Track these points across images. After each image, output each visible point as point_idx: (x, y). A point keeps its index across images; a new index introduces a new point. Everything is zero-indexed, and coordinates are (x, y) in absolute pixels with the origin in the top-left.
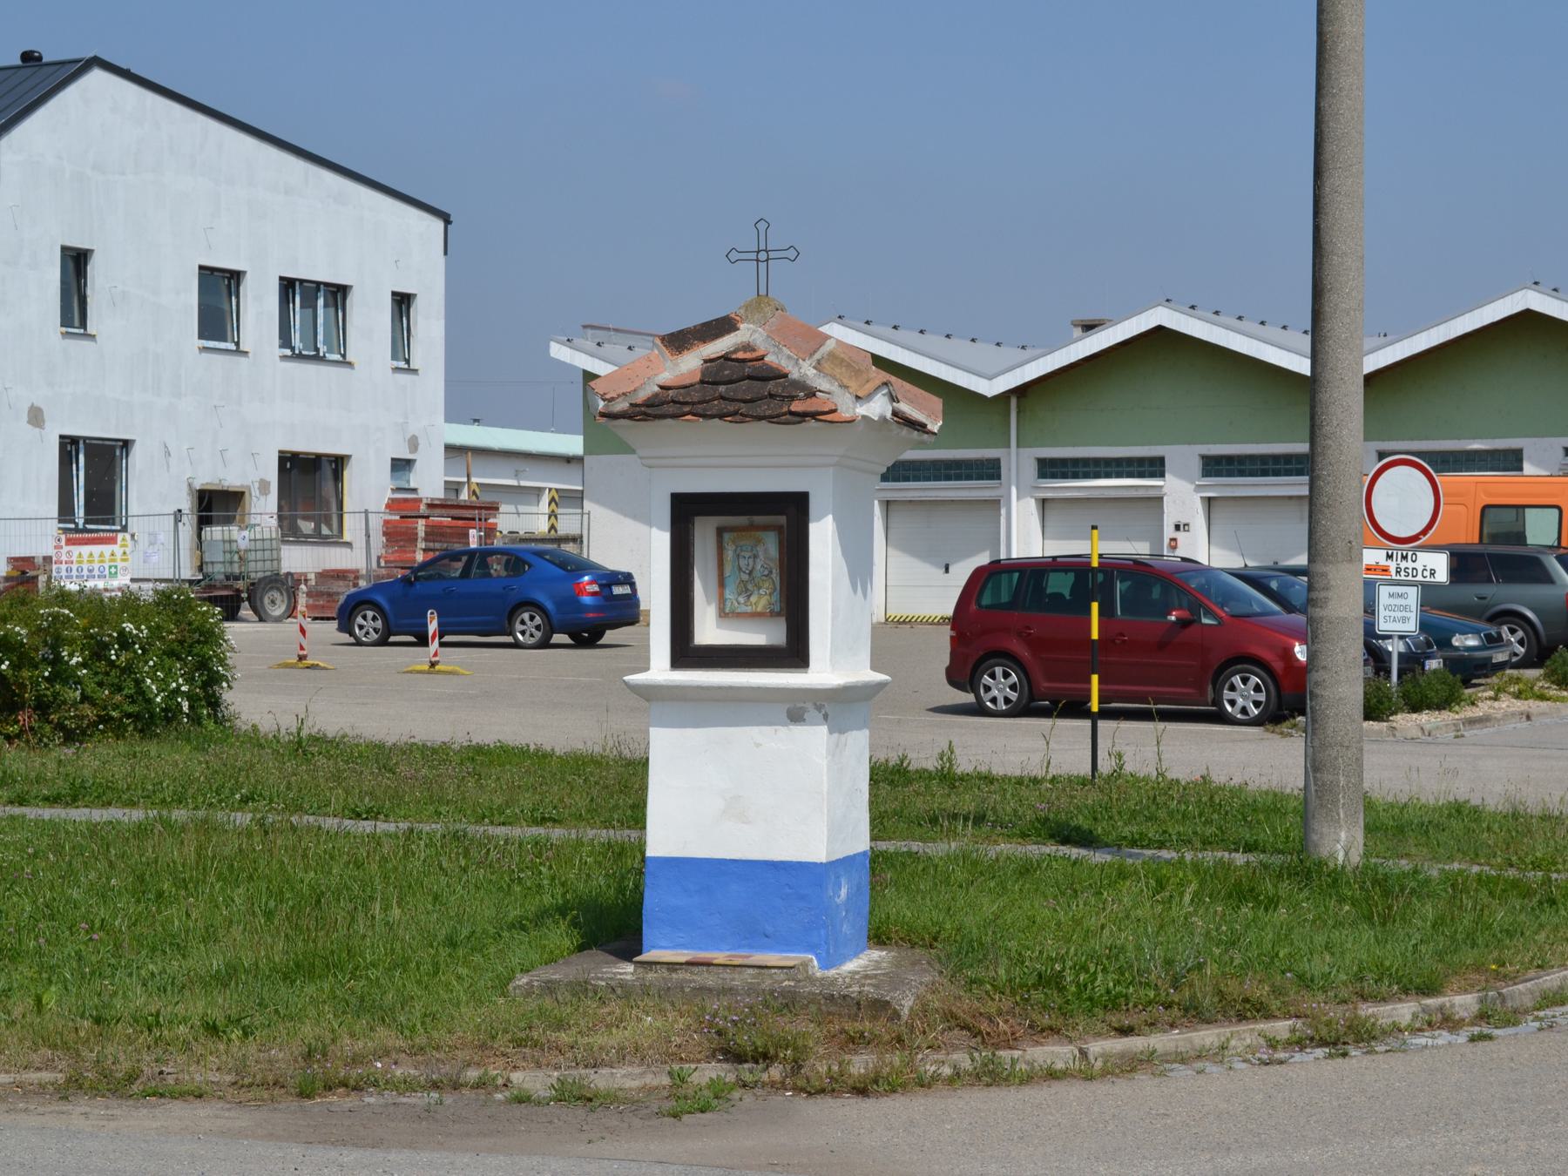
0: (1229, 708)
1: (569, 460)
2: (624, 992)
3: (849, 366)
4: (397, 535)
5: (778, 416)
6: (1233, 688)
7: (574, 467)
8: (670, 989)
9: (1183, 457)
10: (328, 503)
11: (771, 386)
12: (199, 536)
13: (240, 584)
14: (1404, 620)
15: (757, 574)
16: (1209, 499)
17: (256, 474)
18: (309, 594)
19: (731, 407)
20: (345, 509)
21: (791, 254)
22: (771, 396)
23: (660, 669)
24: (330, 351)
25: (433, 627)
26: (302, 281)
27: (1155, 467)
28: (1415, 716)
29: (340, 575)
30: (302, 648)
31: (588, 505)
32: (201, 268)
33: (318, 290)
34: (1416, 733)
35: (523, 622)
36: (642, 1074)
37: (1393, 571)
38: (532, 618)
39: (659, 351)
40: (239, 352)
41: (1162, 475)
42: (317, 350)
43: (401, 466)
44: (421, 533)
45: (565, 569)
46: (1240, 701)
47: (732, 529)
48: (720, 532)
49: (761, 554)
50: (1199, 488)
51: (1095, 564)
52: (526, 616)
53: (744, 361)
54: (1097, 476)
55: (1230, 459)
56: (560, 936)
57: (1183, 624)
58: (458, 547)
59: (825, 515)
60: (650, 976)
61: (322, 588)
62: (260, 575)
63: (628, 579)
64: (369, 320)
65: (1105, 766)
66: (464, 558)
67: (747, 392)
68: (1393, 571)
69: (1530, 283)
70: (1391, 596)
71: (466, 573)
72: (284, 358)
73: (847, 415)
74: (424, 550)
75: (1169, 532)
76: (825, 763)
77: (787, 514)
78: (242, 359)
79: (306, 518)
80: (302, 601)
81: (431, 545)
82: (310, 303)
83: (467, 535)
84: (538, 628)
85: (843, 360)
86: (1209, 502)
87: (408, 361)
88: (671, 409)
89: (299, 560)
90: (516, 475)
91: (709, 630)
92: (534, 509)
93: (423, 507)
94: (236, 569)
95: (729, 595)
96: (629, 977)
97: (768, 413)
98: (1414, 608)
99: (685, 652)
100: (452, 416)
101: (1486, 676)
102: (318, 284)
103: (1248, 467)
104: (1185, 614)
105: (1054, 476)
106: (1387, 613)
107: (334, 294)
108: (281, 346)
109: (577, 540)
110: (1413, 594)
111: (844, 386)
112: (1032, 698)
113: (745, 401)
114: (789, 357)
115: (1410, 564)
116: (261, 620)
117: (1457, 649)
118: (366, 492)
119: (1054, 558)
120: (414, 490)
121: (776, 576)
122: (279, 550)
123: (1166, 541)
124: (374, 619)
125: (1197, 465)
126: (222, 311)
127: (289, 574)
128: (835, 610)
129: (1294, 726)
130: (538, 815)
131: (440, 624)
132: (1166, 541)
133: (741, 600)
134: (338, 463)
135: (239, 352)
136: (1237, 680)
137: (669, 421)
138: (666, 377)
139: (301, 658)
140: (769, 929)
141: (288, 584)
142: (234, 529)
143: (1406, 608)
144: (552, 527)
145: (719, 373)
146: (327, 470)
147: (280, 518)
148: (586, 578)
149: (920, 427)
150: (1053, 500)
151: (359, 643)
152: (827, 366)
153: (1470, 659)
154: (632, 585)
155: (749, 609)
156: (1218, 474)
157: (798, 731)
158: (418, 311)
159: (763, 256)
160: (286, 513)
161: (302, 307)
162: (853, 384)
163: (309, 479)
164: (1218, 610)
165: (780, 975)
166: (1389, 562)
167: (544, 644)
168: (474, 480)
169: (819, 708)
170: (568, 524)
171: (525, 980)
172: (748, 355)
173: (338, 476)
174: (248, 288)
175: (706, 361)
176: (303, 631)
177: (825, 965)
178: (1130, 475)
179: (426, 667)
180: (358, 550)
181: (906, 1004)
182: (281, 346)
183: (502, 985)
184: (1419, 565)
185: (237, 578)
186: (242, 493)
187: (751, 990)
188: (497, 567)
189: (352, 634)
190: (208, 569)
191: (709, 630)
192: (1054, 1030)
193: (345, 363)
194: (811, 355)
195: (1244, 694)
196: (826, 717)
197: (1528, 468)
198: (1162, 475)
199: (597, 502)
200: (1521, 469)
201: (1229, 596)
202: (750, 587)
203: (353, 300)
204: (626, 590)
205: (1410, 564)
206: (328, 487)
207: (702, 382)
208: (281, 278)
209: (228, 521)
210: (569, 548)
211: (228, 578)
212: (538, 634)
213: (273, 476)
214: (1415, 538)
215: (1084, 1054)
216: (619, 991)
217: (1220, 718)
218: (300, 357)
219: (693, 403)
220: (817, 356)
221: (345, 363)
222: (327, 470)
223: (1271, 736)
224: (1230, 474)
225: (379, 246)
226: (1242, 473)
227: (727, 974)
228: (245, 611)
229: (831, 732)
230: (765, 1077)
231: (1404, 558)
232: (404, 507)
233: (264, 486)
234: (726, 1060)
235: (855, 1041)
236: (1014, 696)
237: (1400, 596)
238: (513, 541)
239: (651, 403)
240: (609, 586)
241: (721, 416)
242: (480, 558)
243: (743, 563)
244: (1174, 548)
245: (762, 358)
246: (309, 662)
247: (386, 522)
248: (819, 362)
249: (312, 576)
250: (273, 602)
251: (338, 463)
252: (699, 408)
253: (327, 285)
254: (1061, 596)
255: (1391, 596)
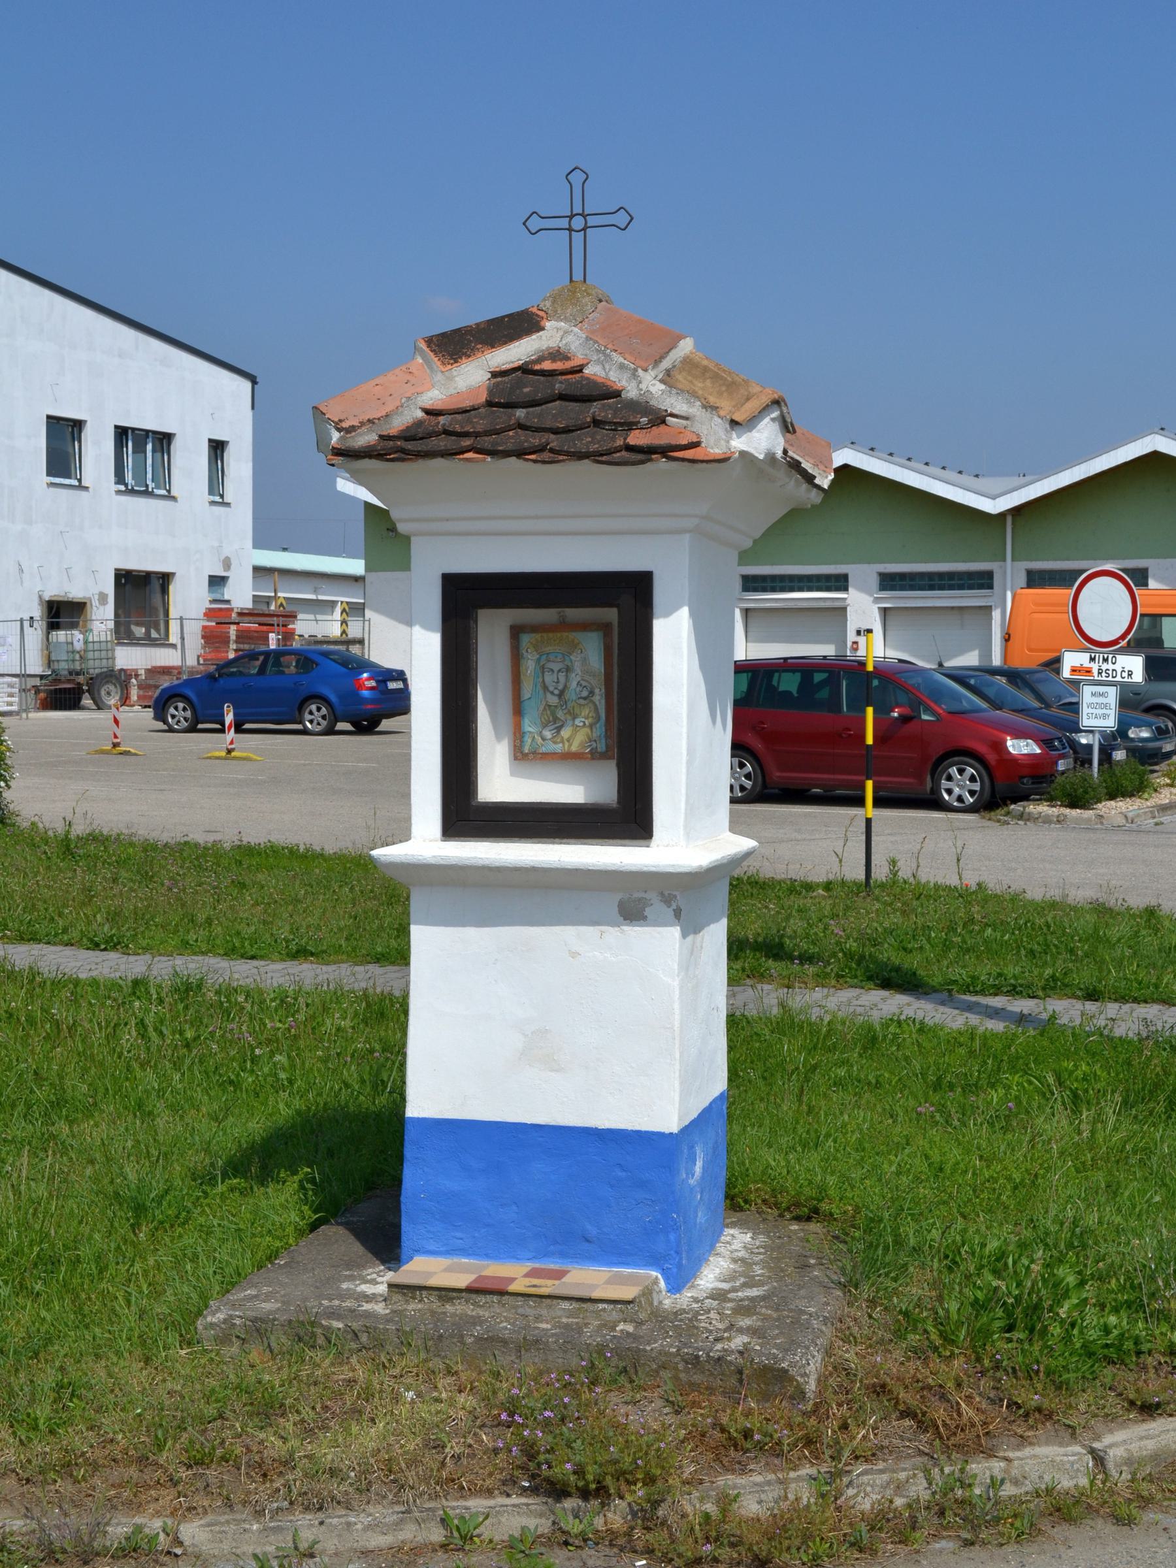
0: (946, 797)
1: (357, 579)
2: (369, 1340)
3: (716, 377)
4: (213, 638)
5: (609, 452)
6: (950, 778)
7: (360, 584)
8: (438, 1336)
9: (864, 573)
10: (156, 609)
11: (595, 408)
12: (48, 639)
13: (81, 679)
14: (1105, 716)
15: (571, 695)
16: (885, 609)
17: (95, 586)
18: (140, 687)
19: (535, 440)
20: (171, 616)
21: (621, 219)
22: (597, 423)
23: (425, 841)
24: (158, 487)
25: (229, 718)
26: (133, 429)
27: (840, 582)
28: (1112, 802)
29: (166, 671)
30: (116, 737)
31: (368, 613)
32: (49, 417)
33: (147, 437)
34: (1121, 821)
35: (311, 713)
36: (398, 1525)
37: (1095, 672)
38: (319, 709)
39: (422, 361)
40: (81, 487)
41: (846, 589)
42: (147, 486)
43: (217, 582)
44: (233, 637)
45: (347, 667)
46: (957, 790)
47: (534, 629)
48: (516, 632)
49: (577, 667)
50: (877, 600)
51: (870, 668)
52: (314, 707)
53: (552, 373)
54: (792, 590)
55: (902, 576)
56: (283, 1201)
57: (905, 720)
58: (263, 648)
59: (677, 608)
60: (413, 1306)
61: (151, 682)
62: (97, 671)
63: (400, 676)
64: (189, 464)
65: (880, 872)
66: (261, 658)
67: (558, 419)
68: (1095, 672)
69: (1157, 429)
70: (1093, 695)
71: (262, 670)
72: (119, 492)
73: (716, 451)
74: (236, 651)
75: (851, 636)
76: (676, 983)
77: (626, 600)
78: (84, 493)
79: (138, 624)
80: (134, 694)
81: (241, 646)
82: (140, 449)
83: (268, 638)
84: (324, 717)
85: (706, 369)
86: (885, 612)
87: (222, 496)
88: (442, 443)
89: (130, 658)
90: (315, 591)
91: (499, 781)
92: (329, 618)
93: (234, 615)
94: (77, 666)
95: (528, 726)
96: (380, 1308)
97: (594, 447)
98: (1113, 706)
99: (464, 814)
100: (259, 543)
101: (1156, 764)
102: (147, 432)
103: (937, 582)
104: (907, 711)
105: (755, 590)
106: (1090, 711)
107: (161, 441)
108: (116, 483)
109: (361, 642)
110: (1112, 692)
111: (709, 407)
112: (765, 785)
113: (556, 431)
114: (622, 367)
115: (1110, 666)
116: (99, 708)
117: (1132, 740)
118: (188, 603)
119: (785, 659)
120: (228, 602)
121: (599, 698)
122: (113, 650)
123: (849, 644)
124: (184, 709)
125: (874, 581)
126: (67, 453)
127: (122, 670)
128: (690, 751)
129: (1008, 813)
130: (293, 947)
131: (235, 715)
132: (849, 644)
133: (548, 734)
134: (165, 579)
135: (81, 487)
136: (954, 771)
137: (439, 462)
138: (434, 397)
139: (115, 745)
140: (592, 1230)
141: (121, 679)
142: (76, 632)
143: (1106, 706)
144: (344, 632)
145: (509, 390)
146: (156, 584)
147: (117, 624)
148: (365, 675)
149: (809, 478)
150: (754, 609)
151: (171, 730)
152: (680, 378)
153: (1143, 749)
154: (405, 681)
155: (558, 748)
156: (893, 588)
157: (635, 934)
158: (230, 455)
159: (578, 223)
160: (122, 619)
161: (134, 452)
162: (726, 405)
163: (141, 592)
164: (936, 707)
165: (613, 1313)
166: (1092, 665)
167: (330, 731)
168: (279, 594)
169: (667, 900)
170: (354, 631)
171: (221, 1316)
172: (559, 366)
173: (165, 590)
174: (88, 434)
175: (495, 375)
176: (116, 721)
177: (676, 1287)
178: (819, 589)
179: (223, 754)
180: (183, 649)
181: (810, 1369)
182: (116, 483)
183: (184, 1324)
184: (1118, 667)
185: (78, 674)
186: (85, 604)
187: (570, 1337)
188: (291, 666)
189: (165, 722)
190: (56, 666)
191: (499, 781)
192: (1045, 1415)
193: (170, 497)
194: (657, 363)
195: (960, 783)
196: (678, 914)
197: (1152, 584)
198: (846, 589)
199: (377, 610)
200: (1147, 585)
201: (938, 693)
202: (560, 714)
203: (177, 446)
204: (400, 685)
205: (1110, 666)
206: (157, 599)
207: (490, 404)
208: (116, 427)
209: (73, 626)
210: (355, 650)
211: (71, 673)
212: (324, 723)
213: (110, 590)
214: (1114, 642)
215: (1099, 1459)
216: (364, 1338)
217: (934, 803)
218: (131, 492)
219: (477, 435)
220: (666, 364)
221: (170, 497)
222: (156, 584)
223: (989, 823)
224: (902, 588)
225: (201, 402)
226: (912, 588)
227: (529, 1309)
228: (87, 701)
229: (684, 935)
230: (599, 1522)
231: (1105, 660)
232: (219, 615)
233: (103, 598)
234: (534, 1491)
235: (735, 1447)
236: (748, 784)
237: (1101, 695)
238: (309, 643)
239: (411, 435)
240: (384, 682)
241: (520, 454)
242: (276, 657)
243: (549, 679)
244: (856, 649)
245: (579, 370)
246: (122, 748)
247: (204, 627)
248: (668, 373)
249: (143, 672)
250: (109, 694)
251: (165, 579)
252: (487, 442)
253: (154, 432)
254: (789, 693)
255: (1093, 695)
